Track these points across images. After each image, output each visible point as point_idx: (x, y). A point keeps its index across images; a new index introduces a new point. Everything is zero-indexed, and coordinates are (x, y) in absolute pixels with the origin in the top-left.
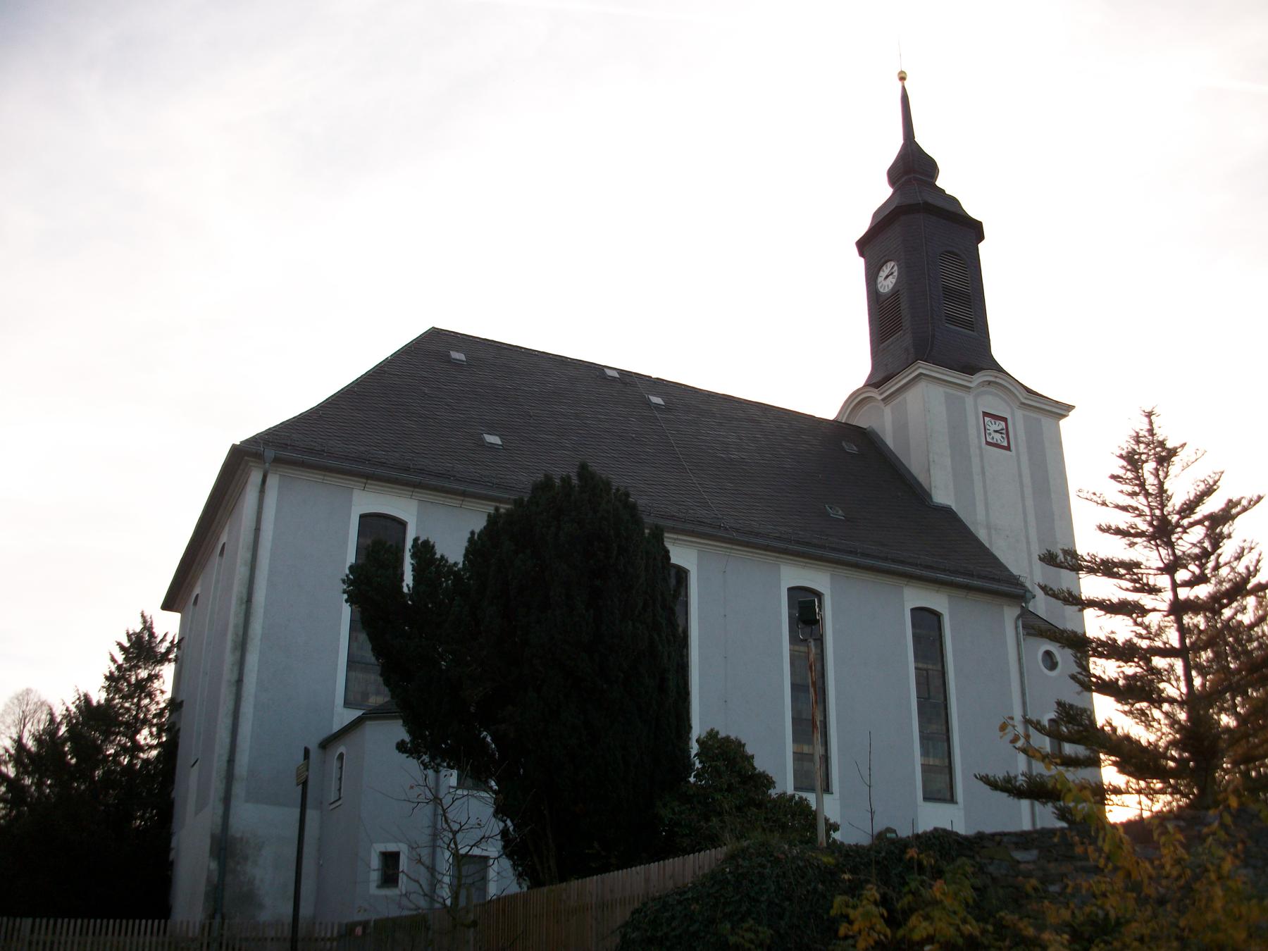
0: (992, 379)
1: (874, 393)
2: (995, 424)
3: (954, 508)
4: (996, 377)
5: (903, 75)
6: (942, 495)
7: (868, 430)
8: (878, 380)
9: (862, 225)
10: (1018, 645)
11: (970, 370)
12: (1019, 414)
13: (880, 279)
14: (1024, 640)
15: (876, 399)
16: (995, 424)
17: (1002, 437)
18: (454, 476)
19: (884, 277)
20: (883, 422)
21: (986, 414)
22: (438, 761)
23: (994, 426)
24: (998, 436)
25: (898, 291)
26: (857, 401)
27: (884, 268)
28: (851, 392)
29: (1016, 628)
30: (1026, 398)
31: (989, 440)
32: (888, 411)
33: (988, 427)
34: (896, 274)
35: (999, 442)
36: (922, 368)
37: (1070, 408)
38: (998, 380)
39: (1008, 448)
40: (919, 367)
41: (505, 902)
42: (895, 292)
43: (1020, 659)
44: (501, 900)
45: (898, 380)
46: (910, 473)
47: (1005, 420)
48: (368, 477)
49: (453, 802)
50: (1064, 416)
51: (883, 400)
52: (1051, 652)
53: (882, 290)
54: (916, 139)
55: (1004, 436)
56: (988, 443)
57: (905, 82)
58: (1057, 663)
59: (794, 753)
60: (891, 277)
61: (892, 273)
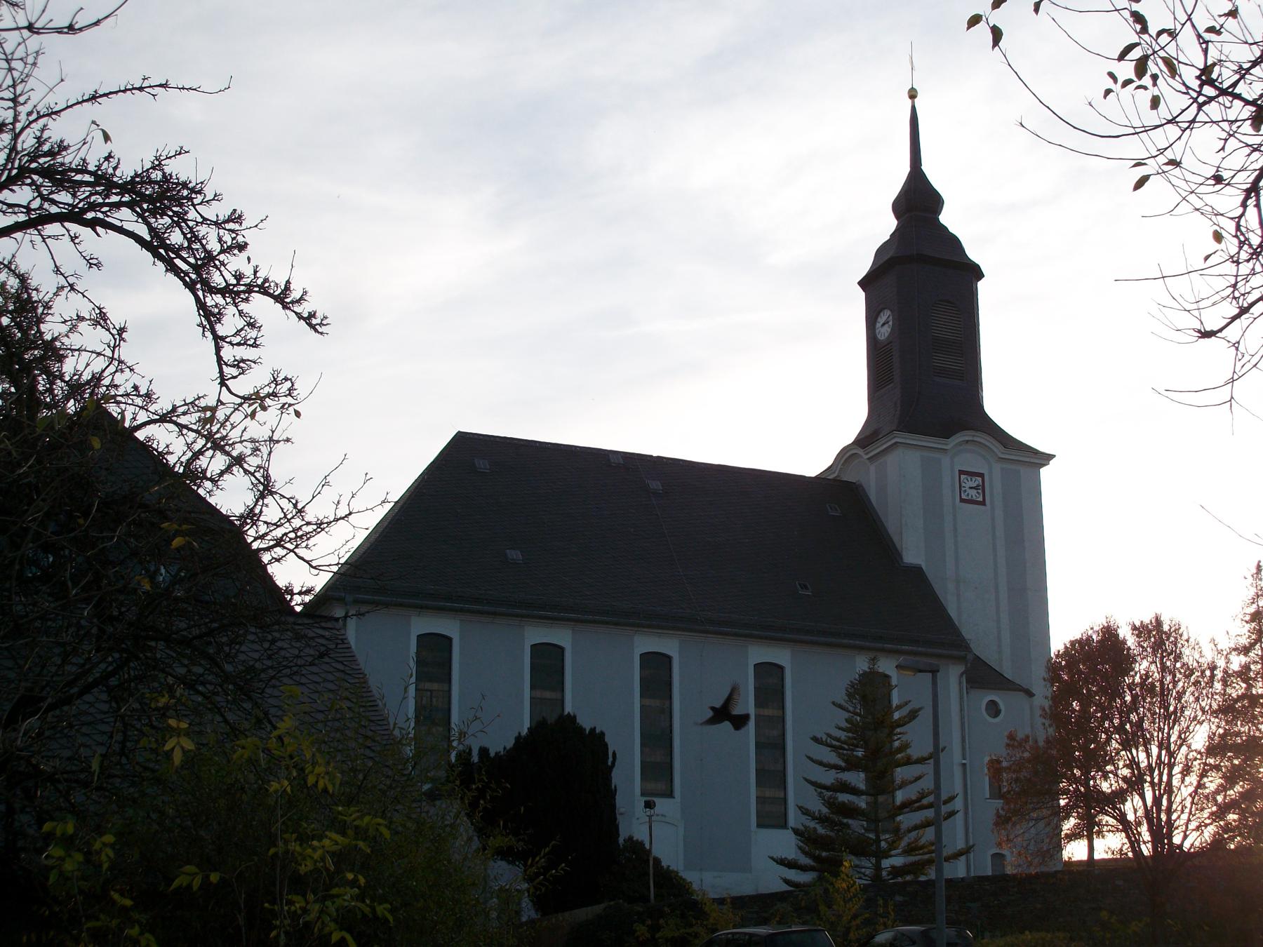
0: (971, 438)
1: (860, 451)
2: (971, 480)
3: (924, 568)
4: (974, 436)
5: (913, 93)
6: (912, 555)
7: (857, 483)
8: (865, 440)
9: (864, 265)
10: (961, 698)
11: (946, 431)
12: (997, 468)
13: (878, 325)
14: (967, 693)
15: (861, 456)
16: (971, 480)
17: (978, 492)
18: (486, 600)
19: (881, 323)
20: (867, 476)
21: (961, 472)
22: (496, 857)
23: (969, 483)
24: (973, 492)
25: (891, 342)
26: (846, 456)
27: (882, 314)
28: (844, 446)
29: (960, 683)
30: (1003, 453)
31: (964, 497)
32: (872, 468)
33: (963, 484)
34: (891, 323)
35: (974, 497)
36: (901, 437)
37: (1051, 457)
38: (975, 439)
39: (983, 503)
40: (895, 437)
41: (532, 922)
42: (889, 342)
43: (962, 710)
44: (13, 441)
45: (876, 446)
46: (887, 531)
47: (982, 475)
48: (422, 608)
49: (313, 497)
50: (1044, 465)
51: (868, 459)
52: (998, 703)
53: (879, 337)
54: (922, 167)
55: (980, 491)
56: (962, 500)
57: (916, 100)
58: (1000, 710)
59: (757, 797)
60: (886, 325)
61: (888, 322)
